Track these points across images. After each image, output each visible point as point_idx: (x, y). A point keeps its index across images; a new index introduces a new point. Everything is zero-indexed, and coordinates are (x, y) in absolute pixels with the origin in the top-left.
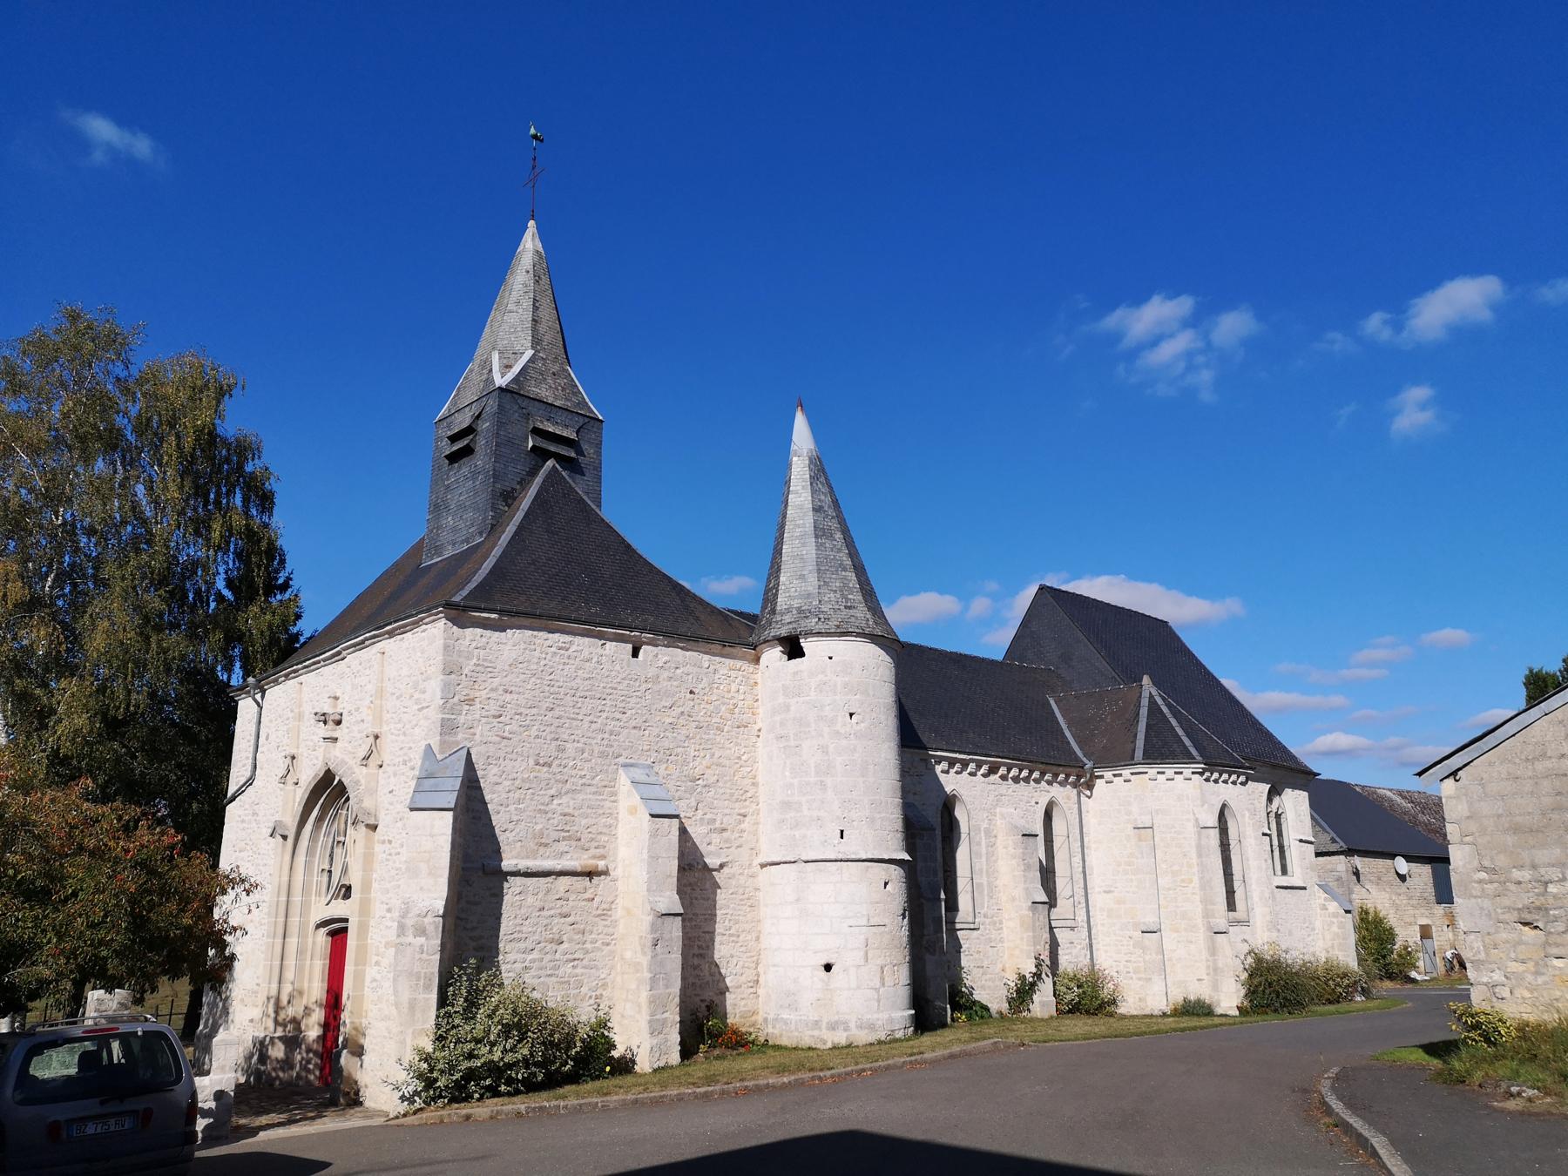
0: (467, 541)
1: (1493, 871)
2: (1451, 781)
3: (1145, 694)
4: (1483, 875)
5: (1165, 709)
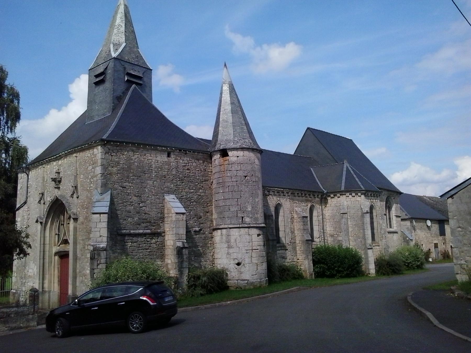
0: (104, 115)
1: (463, 228)
2: (450, 199)
3: (345, 166)
4: (460, 229)
5: (352, 172)
